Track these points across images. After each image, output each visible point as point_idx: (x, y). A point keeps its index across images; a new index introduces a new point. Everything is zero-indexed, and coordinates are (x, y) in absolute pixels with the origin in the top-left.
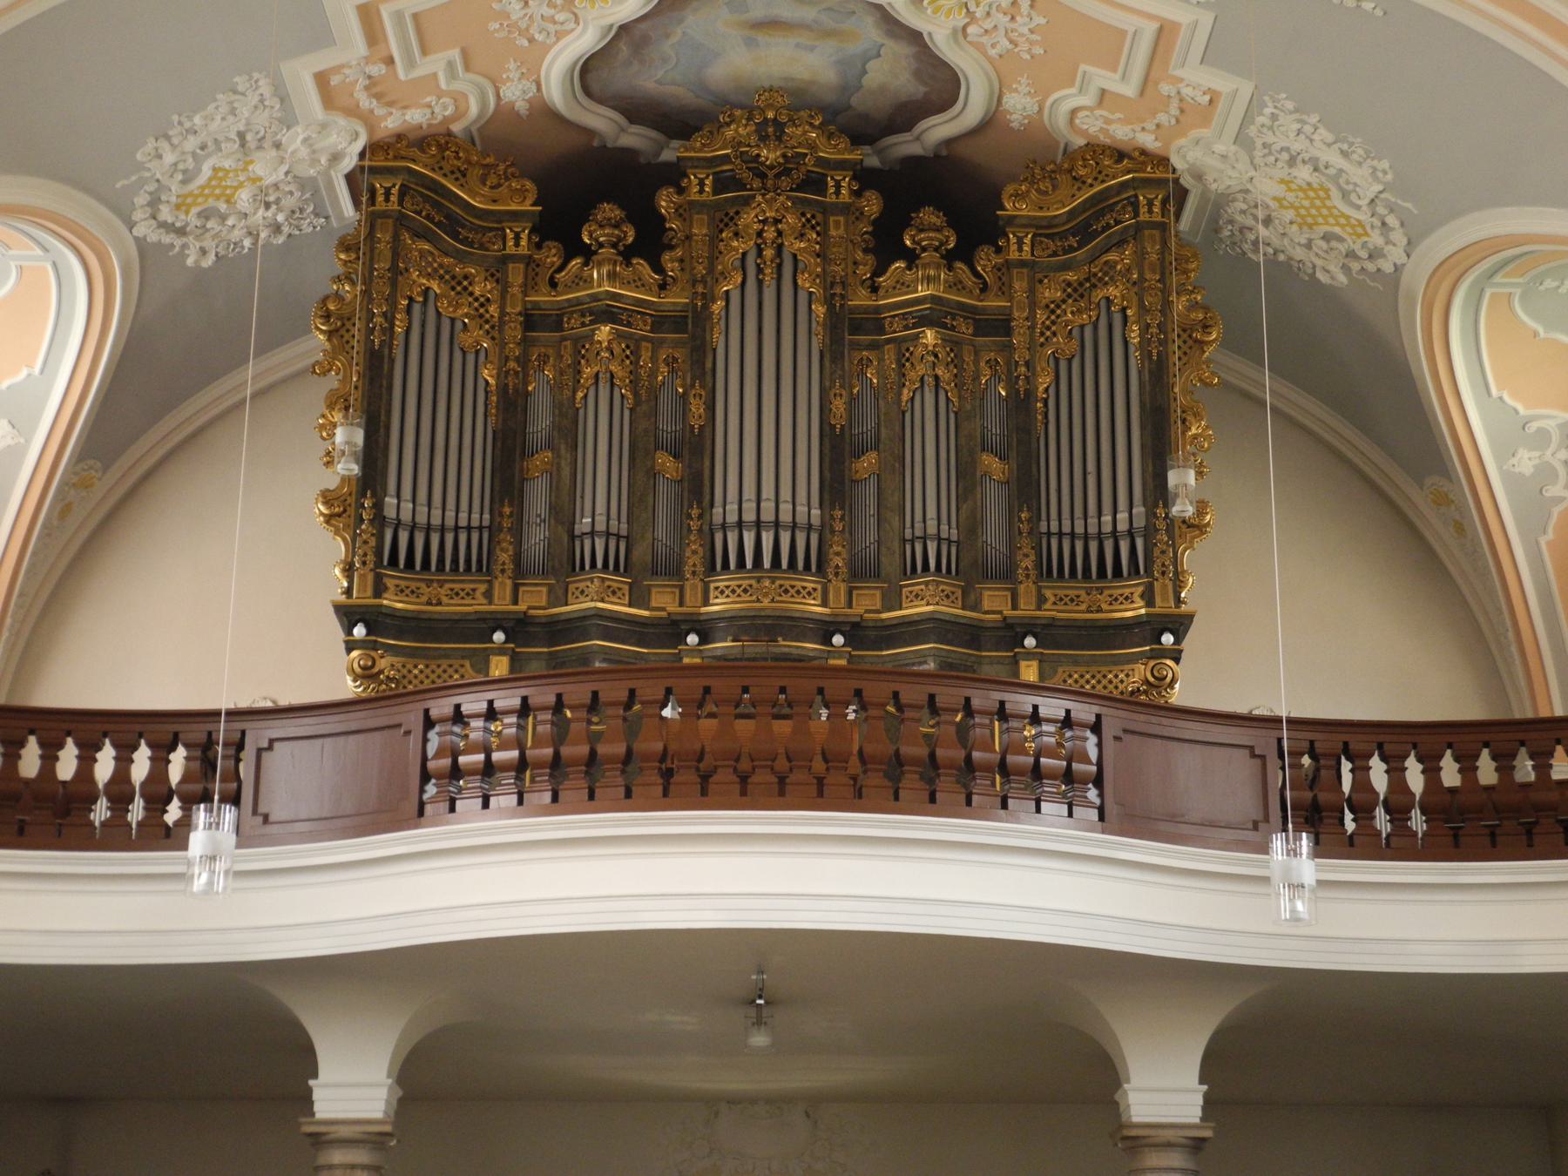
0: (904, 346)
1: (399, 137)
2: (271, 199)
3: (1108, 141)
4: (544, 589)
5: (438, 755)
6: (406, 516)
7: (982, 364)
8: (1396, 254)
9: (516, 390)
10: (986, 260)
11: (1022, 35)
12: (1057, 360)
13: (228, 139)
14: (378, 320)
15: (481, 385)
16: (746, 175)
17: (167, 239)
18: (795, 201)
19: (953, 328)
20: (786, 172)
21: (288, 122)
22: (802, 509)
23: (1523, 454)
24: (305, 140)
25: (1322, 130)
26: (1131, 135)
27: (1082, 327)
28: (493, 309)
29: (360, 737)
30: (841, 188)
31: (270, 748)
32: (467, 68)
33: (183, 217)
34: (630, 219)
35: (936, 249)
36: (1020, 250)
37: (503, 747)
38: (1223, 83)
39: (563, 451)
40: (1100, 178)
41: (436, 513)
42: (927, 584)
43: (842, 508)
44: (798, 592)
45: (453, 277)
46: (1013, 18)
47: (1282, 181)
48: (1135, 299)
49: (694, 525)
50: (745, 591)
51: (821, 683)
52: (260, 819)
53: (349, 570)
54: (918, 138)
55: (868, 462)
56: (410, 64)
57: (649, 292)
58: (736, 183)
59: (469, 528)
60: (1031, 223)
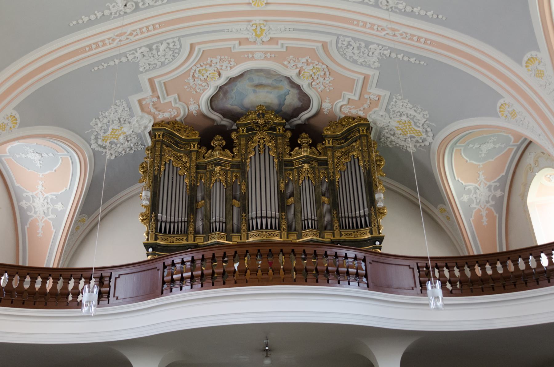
2: (129, 139)
5: (168, 275)
6: (164, 219)
8: (430, 139)
9: (194, 184)
10: (320, 147)
11: (327, 84)
13: (116, 120)
14: (156, 167)
15: (185, 184)
16: (255, 127)
17: (101, 150)
20: (266, 126)
21: (132, 115)
22: (273, 213)
23: (465, 196)
24: (137, 121)
25: (409, 104)
28: (188, 164)
29: (145, 272)
32: (180, 100)
34: (224, 139)
47: (398, 122)
49: (244, 219)
53: (148, 234)
55: (291, 200)
56: (164, 98)
57: (230, 158)
58: (253, 129)
59: (181, 222)
60: (331, 137)
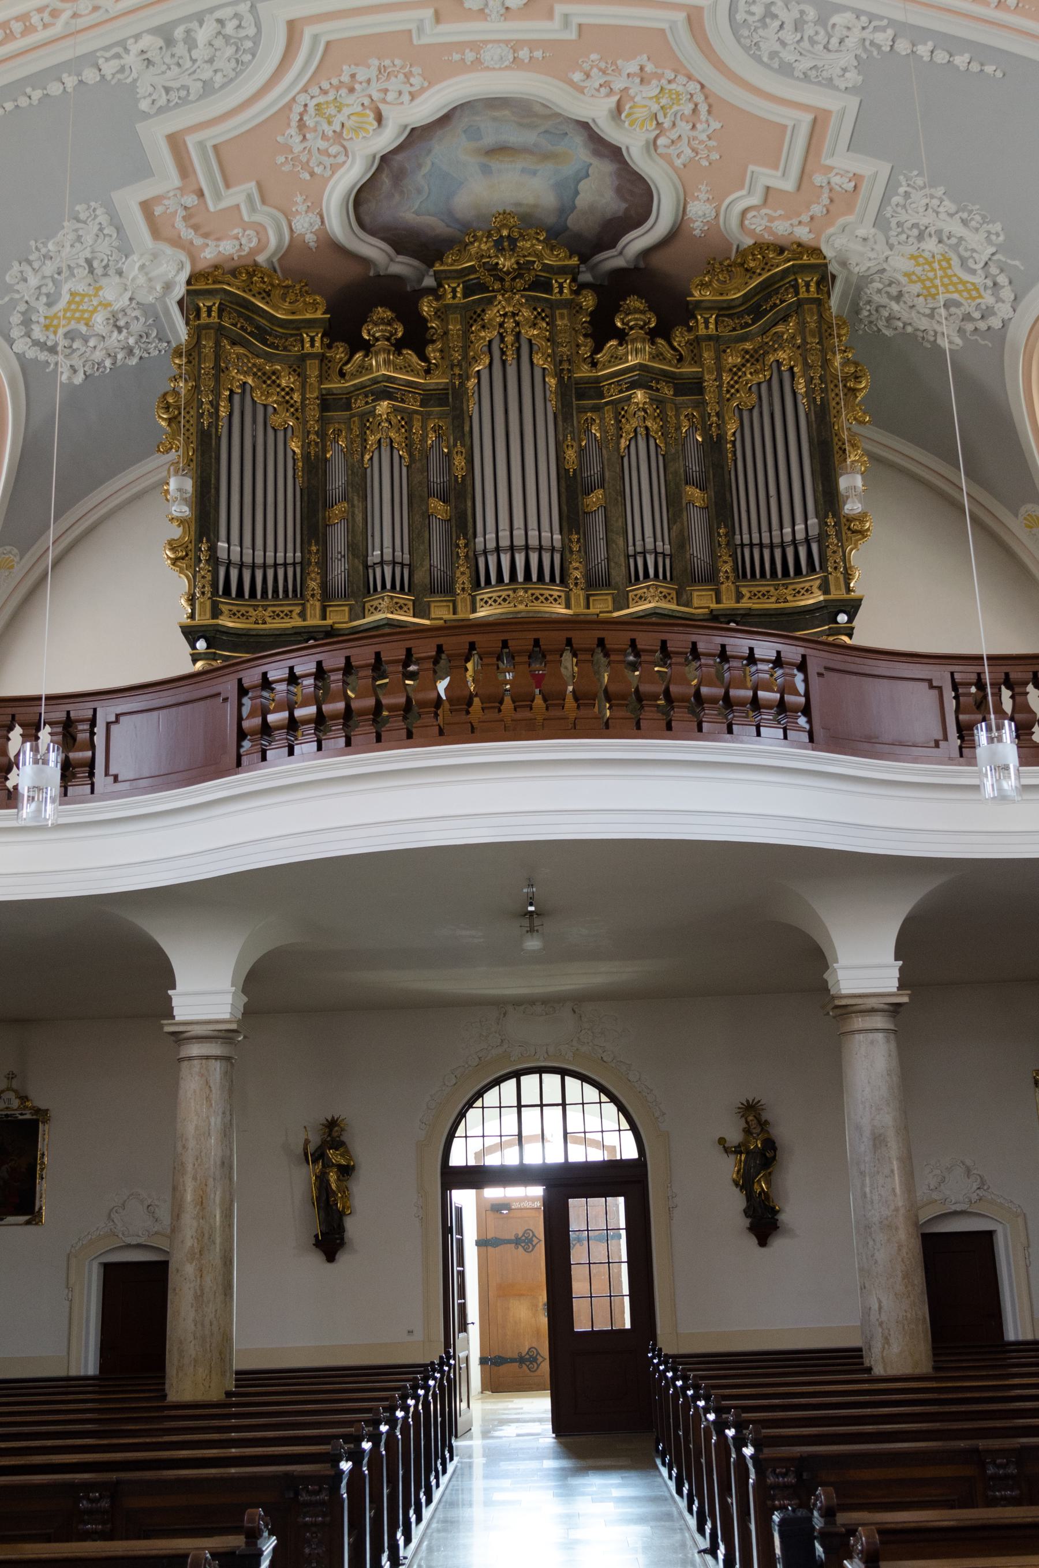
0: (620, 406)
1: (216, 267)
3: (771, 238)
4: (346, 609)
5: (251, 715)
6: (235, 557)
7: (682, 418)
8: (1004, 310)
9: (316, 455)
11: (701, 142)
12: (741, 410)
14: (206, 406)
15: (290, 454)
17: (43, 356)
18: (528, 298)
19: (658, 390)
20: (520, 276)
22: (546, 535)
24: (142, 267)
26: (789, 230)
27: (759, 384)
28: (296, 396)
30: (563, 289)
31: (117, 721)
32: (264, 202)
33: (52, 337)
34: (399, 318)
35: (642, 328)
36: (707, 327)
37: (304, 704)
38: (865, 166)
39: (356, 502)
40: (767, 268)
41: (259, 553)
42: (648, 587)
43: (578, 533)
44: (547, 599)
45: (264, 374)
46: (694, 126)
47: (912, 257)
48: (800, 359)
50: (505, 600)
51: (569, 634)
52: (112, 779)
53: (191, 600)
54: (621, 253)
55: (596, 497)
56: (218, 196)
57: (418, 375)
58: (483, 288)
